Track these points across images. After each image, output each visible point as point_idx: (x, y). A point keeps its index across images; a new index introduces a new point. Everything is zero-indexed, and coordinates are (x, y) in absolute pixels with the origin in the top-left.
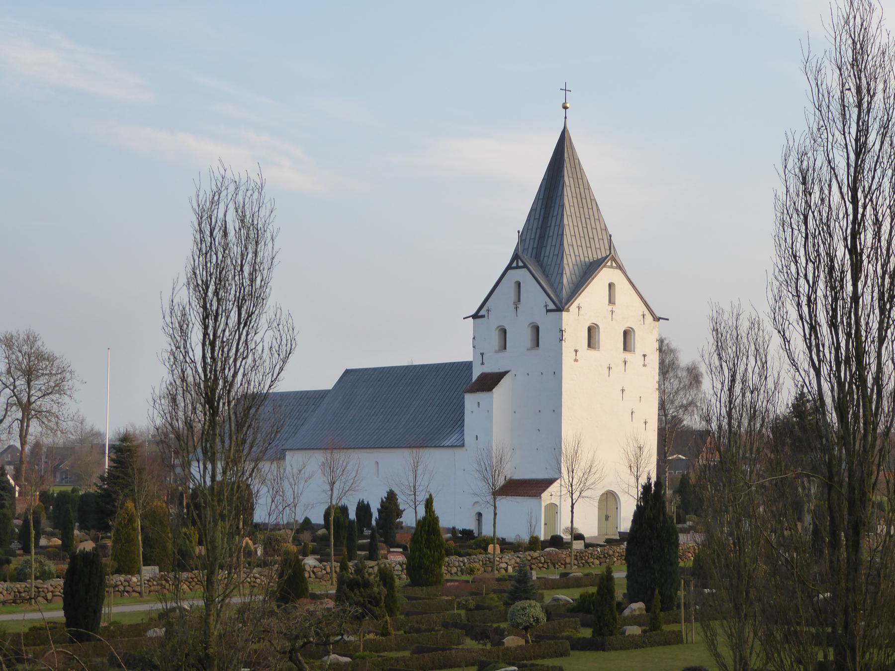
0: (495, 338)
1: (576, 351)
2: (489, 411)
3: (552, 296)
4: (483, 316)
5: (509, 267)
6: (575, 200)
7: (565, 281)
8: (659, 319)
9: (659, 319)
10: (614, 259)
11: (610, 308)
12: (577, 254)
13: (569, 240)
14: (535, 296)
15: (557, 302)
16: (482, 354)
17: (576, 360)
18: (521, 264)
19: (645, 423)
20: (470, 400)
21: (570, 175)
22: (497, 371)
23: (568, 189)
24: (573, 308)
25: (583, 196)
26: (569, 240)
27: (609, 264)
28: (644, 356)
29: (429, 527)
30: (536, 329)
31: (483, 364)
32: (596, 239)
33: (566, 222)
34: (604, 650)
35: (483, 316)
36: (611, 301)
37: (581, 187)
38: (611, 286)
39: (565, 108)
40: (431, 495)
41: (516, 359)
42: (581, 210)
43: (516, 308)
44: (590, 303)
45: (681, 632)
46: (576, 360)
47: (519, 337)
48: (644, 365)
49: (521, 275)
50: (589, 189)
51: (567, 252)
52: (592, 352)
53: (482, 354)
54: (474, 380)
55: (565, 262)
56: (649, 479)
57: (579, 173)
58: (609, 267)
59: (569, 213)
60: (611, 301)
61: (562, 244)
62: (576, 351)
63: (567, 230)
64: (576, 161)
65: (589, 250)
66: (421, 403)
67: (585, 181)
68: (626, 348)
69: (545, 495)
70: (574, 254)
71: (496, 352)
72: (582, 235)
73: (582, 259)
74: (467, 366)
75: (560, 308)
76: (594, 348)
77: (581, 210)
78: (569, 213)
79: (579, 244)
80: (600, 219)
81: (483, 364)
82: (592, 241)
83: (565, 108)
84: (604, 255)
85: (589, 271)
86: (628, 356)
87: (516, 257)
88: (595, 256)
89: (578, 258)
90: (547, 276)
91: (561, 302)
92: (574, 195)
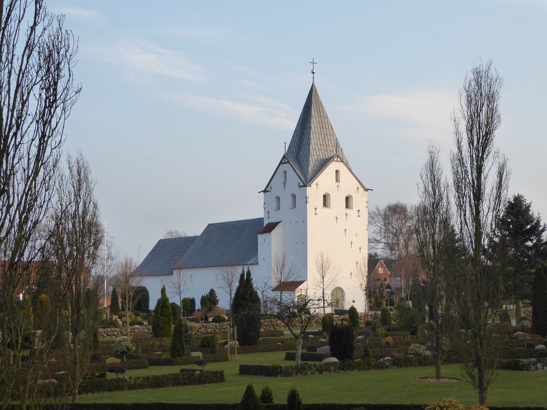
0: (275, 202)
1: (316, 209)
2: (270, 244)
3: (302, 178)
4: (268, 191)
5: (281, 163)
6: (318, 124)
7: (310, 170)
8: (367, 190)
9: (367, 190)
10: (338, 157)
11: (337, 184)
12: (318, 154)
13: (314, 147)
14: (293, 178)
15: (304, 181)
16: (268, 212)
17: (316, 214)
18: (286, 161)
19: (360, 249)
20: (261, 238)
21: (315, 110)
22: (275, 221)
23: (314, 118)
24: (314, 184)
25: (323, 122)
26: (314, 147)
27: (336, 159)
28: (359, 211)
29: (162, 304)
30: (294, 196)
31: (269, 218)
32: (331, 146)
33: (312, 136)
34: (173, 365)
35: (268, 191)
36: (337, 180)
37: (322, 117)
38: (337, 172)
39: (313, 73)
40: (164, 286)
41: (284, 215)
42: (322, 130)
43: (284, 186)
44: (325, 181)
45: (301, 360)
46: (316, 214)
47: (286, 202)
48: (359, 216)
49: (286, 167)
50: (327, 118)
51: (312, 153)
52: (326, 209)
53: (268, 212)
54: (265, 226)
55: (310, 159)
56: (243, 271)
57: (321, 109)
58: (336, 161)
59: (314, 132)
60: (337, 180)
61: (309, 149)
62: (316, 209)
63: (312, 141)
64: (320, 103)
65: (326, 152)
66: (235, 240)
67: (325, 114)
68: (347, 206)
69: (297, 290)
70: (316, 153)
71: (275, 211)
72: (322, 144)
73: (322, 157)
74: (261, 220)
75: (305, 185)
76: (327, 207)
77: (322, 130)
78: (314, 132)
79: (320, 148)
80: (333, 135)
81: (269, 218)
82: (328, 147)
83: (313, 73)
84: (332, 155)
85: (324, 164)
86: (348, 211)
87: (284, 157)
88: (327, 156)
89: (319, 157)
90: (301, 167)
91: (306, 182)
92: (318, 121)
